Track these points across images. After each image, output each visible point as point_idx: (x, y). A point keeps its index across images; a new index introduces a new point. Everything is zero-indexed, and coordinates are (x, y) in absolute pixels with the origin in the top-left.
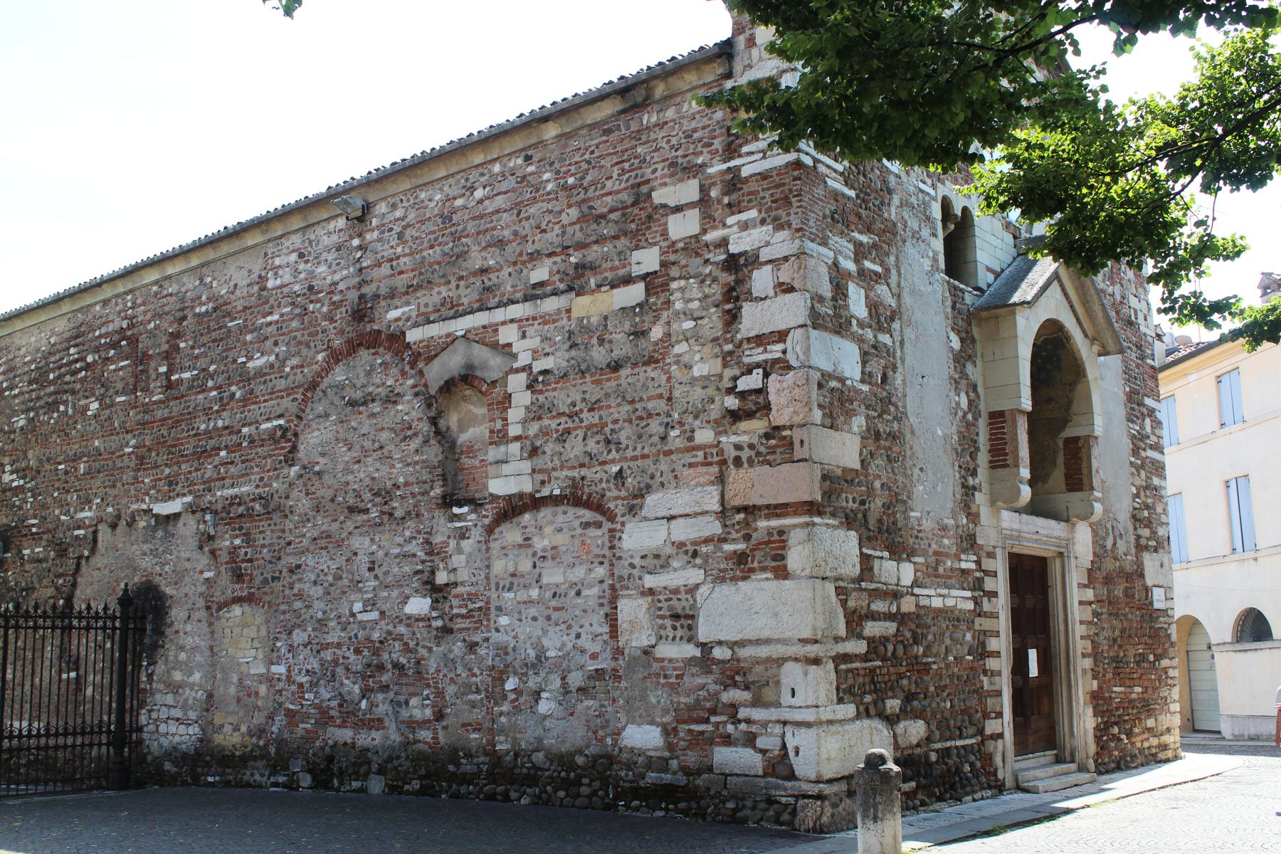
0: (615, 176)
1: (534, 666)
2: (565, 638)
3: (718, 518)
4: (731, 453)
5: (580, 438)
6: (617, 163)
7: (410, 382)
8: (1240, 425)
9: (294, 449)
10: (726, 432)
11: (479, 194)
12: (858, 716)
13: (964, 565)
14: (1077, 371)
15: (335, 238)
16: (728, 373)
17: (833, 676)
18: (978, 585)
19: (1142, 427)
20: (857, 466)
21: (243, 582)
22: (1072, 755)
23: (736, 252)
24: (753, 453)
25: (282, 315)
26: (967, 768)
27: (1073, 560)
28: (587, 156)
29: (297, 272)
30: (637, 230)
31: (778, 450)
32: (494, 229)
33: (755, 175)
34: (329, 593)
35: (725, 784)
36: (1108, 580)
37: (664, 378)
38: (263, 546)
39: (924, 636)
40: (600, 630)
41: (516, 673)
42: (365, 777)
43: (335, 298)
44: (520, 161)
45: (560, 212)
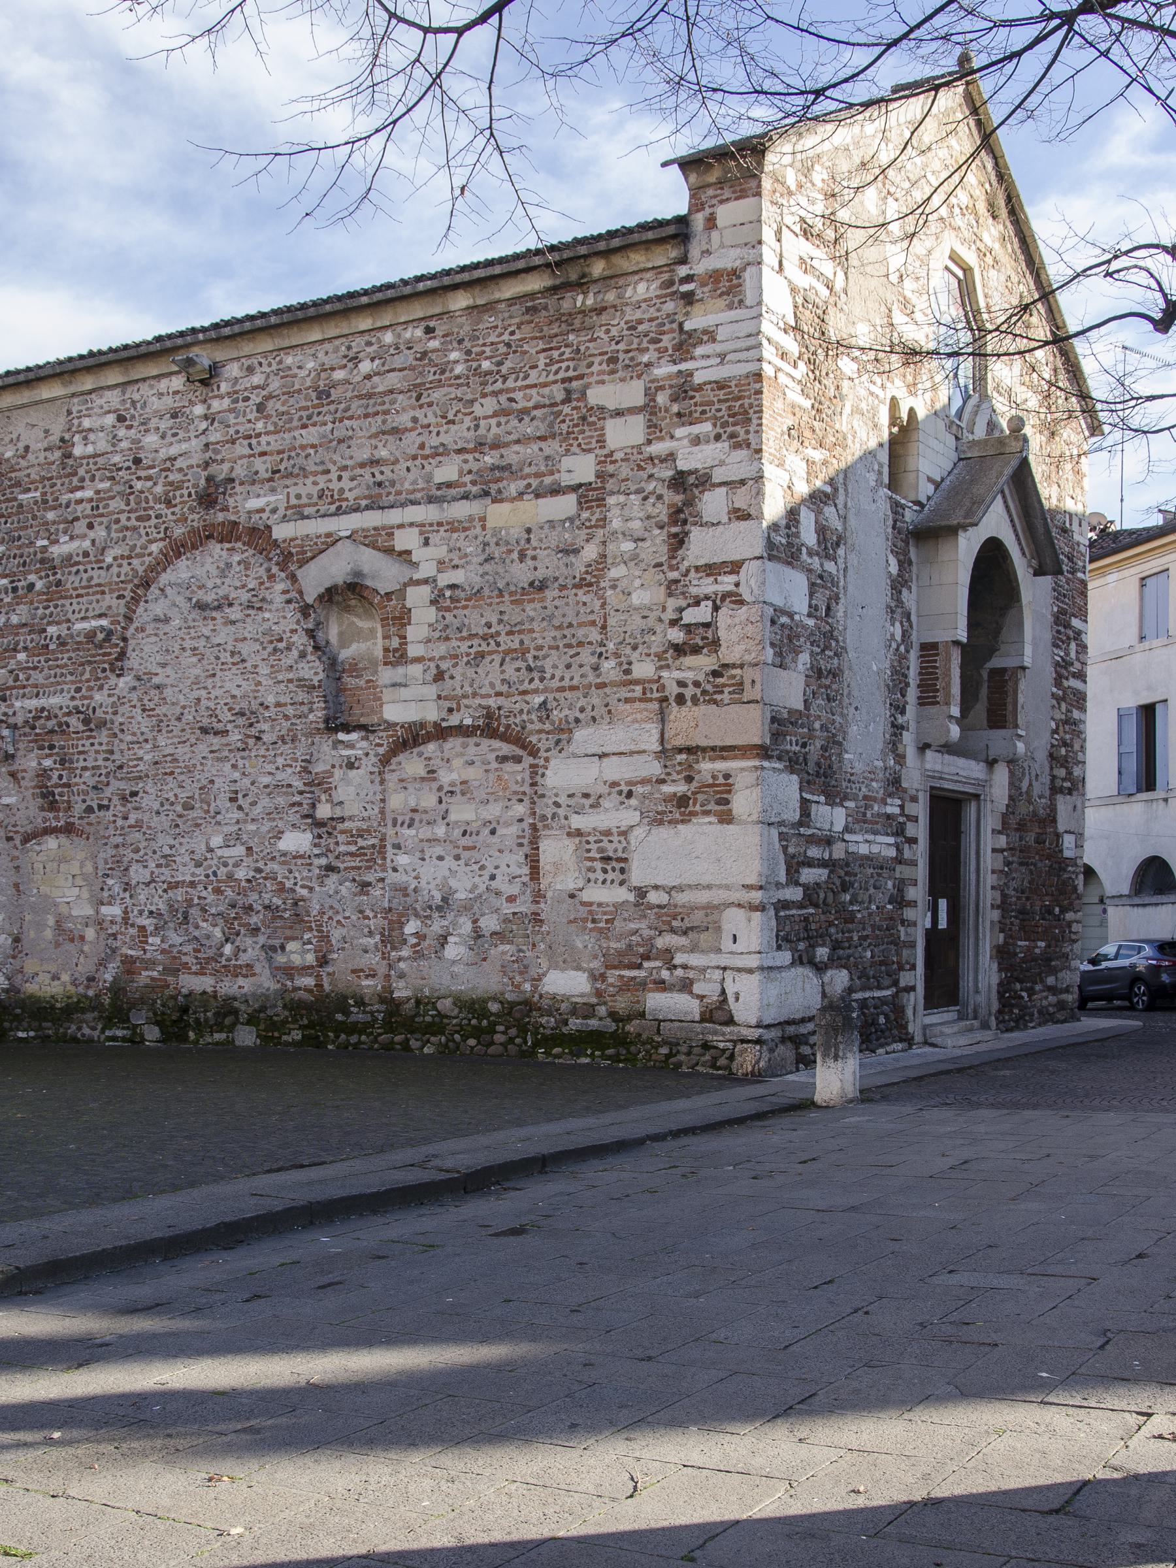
0: (541, 365)
1: (439, 908)
2: (477, 879)
3: (658, 758)
4: (673, 690)
5: (497, 664)
6: (544, 350)
7: (280, 587)
8: (1163, 640)
9: (122, 655)
10: (668, 666)
11: (366, 367)
12: (793, 964)
13: (889, 810)
14: (1011, 594)
15: (168, 402)
16: (672, 603)
17: (774, 923)
18: (900, 831)
19: (1067, 654)
20: (801, 707)
21: (58, 810)
22: (975, 1011)
23: (685, 469)
24: (698, 691)
25: (98, 492)
26: (882, 1020)
27: (989, 804)
28: (506, 337)
29: (115, 440)
30: (568, 433)
31: (726, 690)
32: (386, 412)
33: (710, 383)
34: (177, 826)
35: (659, 1030)
36: (1021, 827)
37: (598, 603)
38: (85, 769)
39: (852, 884)
40: (518, 872)
41: (417, 915)
42: (231, 1028)
43: (171, 478)
44: (419, 333)
45: (472, 402)
